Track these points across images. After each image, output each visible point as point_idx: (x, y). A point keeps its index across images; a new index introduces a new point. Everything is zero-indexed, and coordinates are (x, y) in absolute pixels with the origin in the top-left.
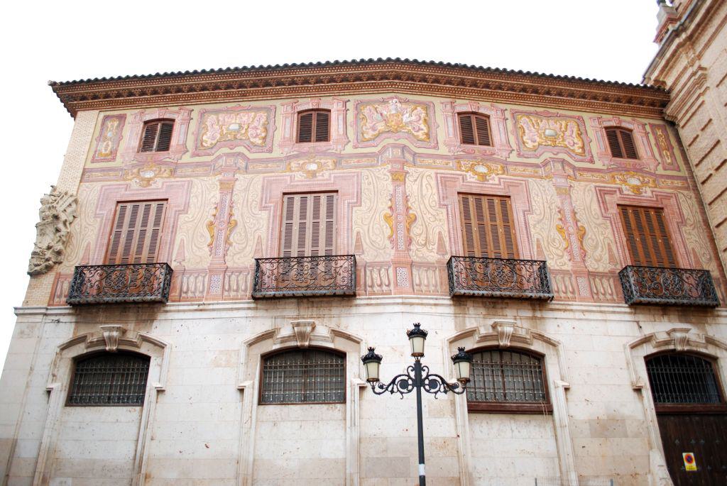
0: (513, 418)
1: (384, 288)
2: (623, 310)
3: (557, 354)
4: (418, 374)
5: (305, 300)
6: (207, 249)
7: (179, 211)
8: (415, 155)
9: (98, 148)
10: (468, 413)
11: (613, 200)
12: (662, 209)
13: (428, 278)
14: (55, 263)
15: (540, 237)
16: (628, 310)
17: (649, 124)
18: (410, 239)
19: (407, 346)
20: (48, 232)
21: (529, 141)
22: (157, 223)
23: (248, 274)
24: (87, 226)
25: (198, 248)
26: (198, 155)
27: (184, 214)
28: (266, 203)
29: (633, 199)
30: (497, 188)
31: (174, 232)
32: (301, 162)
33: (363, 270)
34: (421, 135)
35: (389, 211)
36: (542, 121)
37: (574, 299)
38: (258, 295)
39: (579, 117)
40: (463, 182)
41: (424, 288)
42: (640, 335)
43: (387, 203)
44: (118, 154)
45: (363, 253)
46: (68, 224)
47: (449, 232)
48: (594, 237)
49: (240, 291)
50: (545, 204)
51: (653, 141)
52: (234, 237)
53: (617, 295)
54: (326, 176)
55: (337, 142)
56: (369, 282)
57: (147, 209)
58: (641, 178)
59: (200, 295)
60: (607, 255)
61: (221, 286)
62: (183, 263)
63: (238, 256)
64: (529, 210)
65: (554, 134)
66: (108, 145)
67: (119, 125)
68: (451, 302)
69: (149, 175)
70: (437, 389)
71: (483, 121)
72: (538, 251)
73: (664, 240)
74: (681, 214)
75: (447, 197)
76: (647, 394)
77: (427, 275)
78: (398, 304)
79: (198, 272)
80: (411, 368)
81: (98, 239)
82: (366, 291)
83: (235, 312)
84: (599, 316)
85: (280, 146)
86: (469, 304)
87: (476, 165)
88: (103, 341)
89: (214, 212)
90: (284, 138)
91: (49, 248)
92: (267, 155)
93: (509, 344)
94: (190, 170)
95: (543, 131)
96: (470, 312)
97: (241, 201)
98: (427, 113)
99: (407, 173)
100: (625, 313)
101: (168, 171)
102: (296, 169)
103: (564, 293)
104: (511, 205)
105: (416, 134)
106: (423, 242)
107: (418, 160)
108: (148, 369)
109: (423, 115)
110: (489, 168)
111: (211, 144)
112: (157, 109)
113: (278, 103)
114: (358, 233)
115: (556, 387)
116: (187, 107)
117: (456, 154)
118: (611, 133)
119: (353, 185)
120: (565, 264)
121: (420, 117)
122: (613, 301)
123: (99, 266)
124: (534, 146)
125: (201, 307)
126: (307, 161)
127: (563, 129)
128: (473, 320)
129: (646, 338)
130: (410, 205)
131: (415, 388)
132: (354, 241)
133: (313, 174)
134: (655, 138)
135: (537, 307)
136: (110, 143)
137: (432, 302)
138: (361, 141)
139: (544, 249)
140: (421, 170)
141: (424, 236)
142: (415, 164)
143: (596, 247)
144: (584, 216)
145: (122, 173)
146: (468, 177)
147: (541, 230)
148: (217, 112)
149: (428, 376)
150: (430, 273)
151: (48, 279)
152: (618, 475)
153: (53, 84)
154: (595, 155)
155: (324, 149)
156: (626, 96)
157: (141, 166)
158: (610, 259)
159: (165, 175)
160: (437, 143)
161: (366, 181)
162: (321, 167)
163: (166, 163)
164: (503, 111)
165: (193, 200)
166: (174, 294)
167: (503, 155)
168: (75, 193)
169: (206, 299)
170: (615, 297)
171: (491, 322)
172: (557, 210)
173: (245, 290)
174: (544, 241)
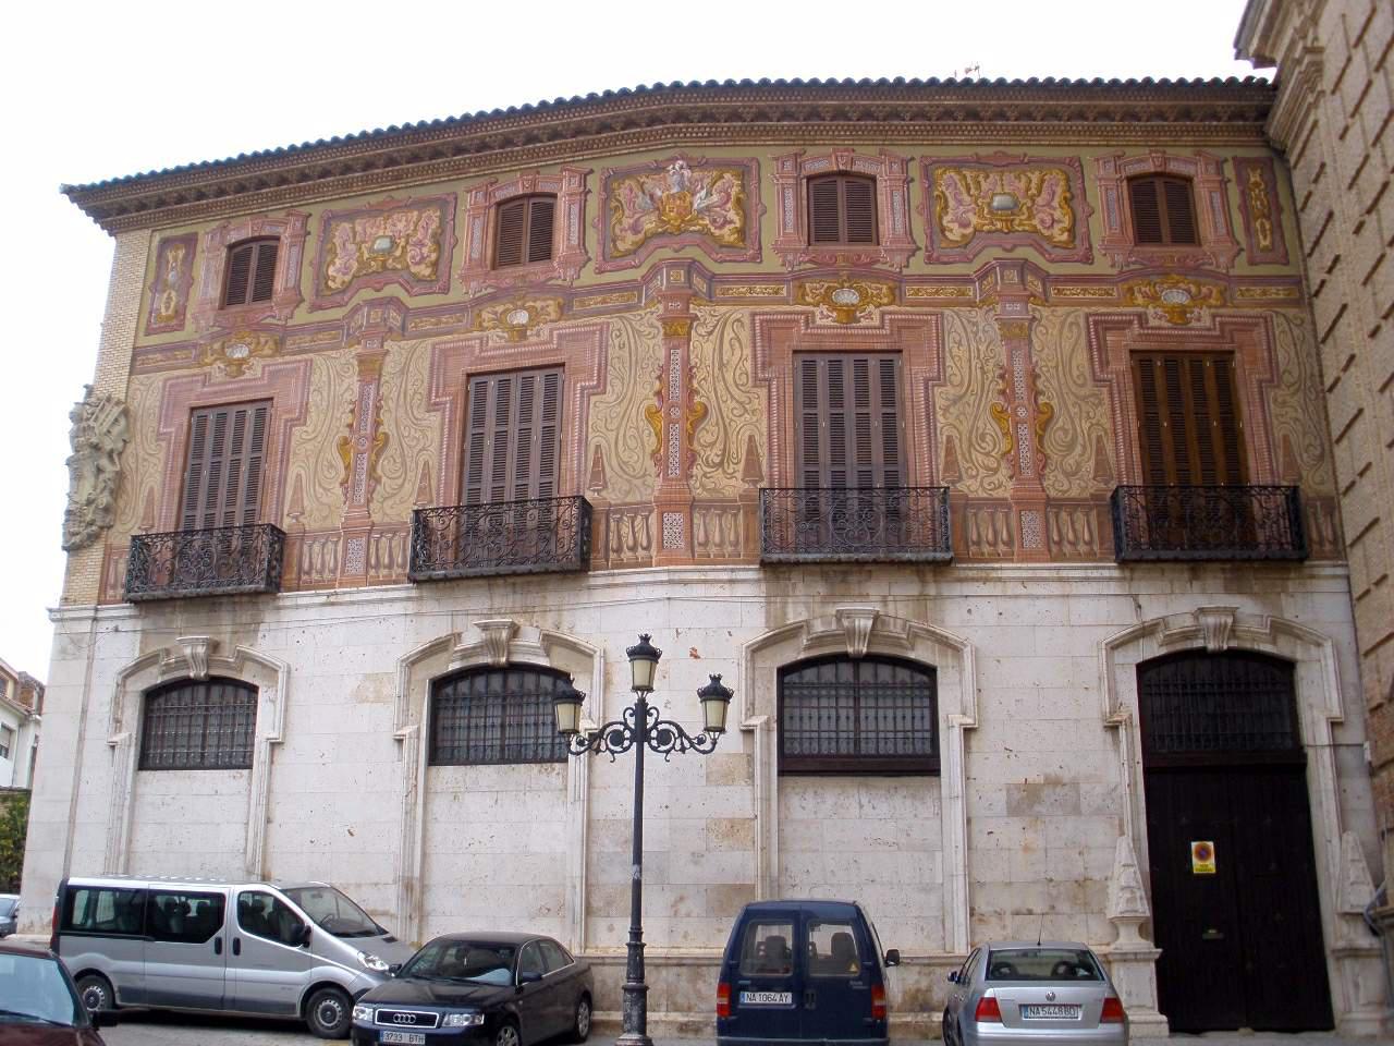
0: (867, 786)
1: (641, 553)
2: (1106, 573)
4: (641, 721)
5: (500, 581)
6: (339, 491)
7: (292, 420)
8: (712, 278)
12: (1231, 352)
13: (721, 530)
14: (102, 528)
15: (955, 433)
16: (1116, 573)
17: (1234, 159)
18: (693, 456)
19: (626, 673)
20: (86, 474)
21: (955, 226)
22: (257, 445)
25: (324, 489)
26: (320, 308)
27: (300, 425)
29: (1167, 335)
31: (285, 461)
33: (603, 521)
34: (727, 234)
35: (655, 401)
36: (987, 177)
38: (420, 576)
39: (1071, 159)
40: (807, 327)
41: (713, 550)
42: (1135, 622)
43: (652, 385)
44: (188, 316)
45: (605, 486)
46: (115, 456)
51: (1235, 198)
52: (384, 466)
53: (1101, 544)
54: (545, 335)
55: (566, 263)
56: (613, 544)
58: (1193, 289)
60: (1092, 463)
62: (301, 519)
63: (390, 502)
64: (939, 379)
66: (169, 298)
67: (187, 254)
68: (761, 575)
69: (240, 353)
70: (670, 745)
71: (862, 188)
72: (946, 463)
73: (1223, 421)
74: (1272, 363)
75: (770, 364)
76: (1132, 738)
78: (662, 582)
79: (328, 535)
82: (607, 561)
84: (1055, 589)
85: (465, 279)
86: (796, 576)
87: (835, 289)
89: (348, 418)
91: (89, 502)
92: (436, 300)
94: (308, 338)
96: (798, 593)
97: (394, 395)
98: (743, 186)
99: (696, 318)
100: (1110, 579)
101: (271, 343)
102: (491, 324)
104: (901, 368)
105: (717, 232)
106: (717, 460)
109: (734, 191)
110: (860, 291)
112: (249, 218)
114: (598, 447)
115: (950, 727)
116: (301, 209)
118: (1142, 189)
119: (593, 351)
121: (729, 195)
122: (1090, 556)
123: (167, 534)
124: (964, 236)
125: (332, 599)
128: (801, 608)
129: (1144, 628)
130: (696, 385)
133: (521, 332)
134: (1243, 193)
135: (929, 577)
136: (173, 294)
137: (725, 576)
138: (611, 258)
139: (960, 457)
140: (723, 309)
141: (718, 449)
142: (711, 298)
143: (1070, 447)
144: (1055, 384)
145: (195, 352)
147: (957, 417)
148: (350, 216)
149: (657, 723)
150: (728, 520)
151: (95, 555)
152: (1051, 880)
153: (69, 191)
154: (1096, 245)
155: (542, 278)
156: (1175, 106)
157: (226, 335)
158: (1096, 471)
159: (267, 351)
160: (760, 248)
161: (616, 342)
162: (535, 316)
163: (267, 328)
164: (905, 163)
165: (314, 398)
167: (890, 261)
168: (122, 397)
169: (341, 585)
170: (1096, 548)
172: (999, 372)
173: (403, 566)
174: (960, 440)
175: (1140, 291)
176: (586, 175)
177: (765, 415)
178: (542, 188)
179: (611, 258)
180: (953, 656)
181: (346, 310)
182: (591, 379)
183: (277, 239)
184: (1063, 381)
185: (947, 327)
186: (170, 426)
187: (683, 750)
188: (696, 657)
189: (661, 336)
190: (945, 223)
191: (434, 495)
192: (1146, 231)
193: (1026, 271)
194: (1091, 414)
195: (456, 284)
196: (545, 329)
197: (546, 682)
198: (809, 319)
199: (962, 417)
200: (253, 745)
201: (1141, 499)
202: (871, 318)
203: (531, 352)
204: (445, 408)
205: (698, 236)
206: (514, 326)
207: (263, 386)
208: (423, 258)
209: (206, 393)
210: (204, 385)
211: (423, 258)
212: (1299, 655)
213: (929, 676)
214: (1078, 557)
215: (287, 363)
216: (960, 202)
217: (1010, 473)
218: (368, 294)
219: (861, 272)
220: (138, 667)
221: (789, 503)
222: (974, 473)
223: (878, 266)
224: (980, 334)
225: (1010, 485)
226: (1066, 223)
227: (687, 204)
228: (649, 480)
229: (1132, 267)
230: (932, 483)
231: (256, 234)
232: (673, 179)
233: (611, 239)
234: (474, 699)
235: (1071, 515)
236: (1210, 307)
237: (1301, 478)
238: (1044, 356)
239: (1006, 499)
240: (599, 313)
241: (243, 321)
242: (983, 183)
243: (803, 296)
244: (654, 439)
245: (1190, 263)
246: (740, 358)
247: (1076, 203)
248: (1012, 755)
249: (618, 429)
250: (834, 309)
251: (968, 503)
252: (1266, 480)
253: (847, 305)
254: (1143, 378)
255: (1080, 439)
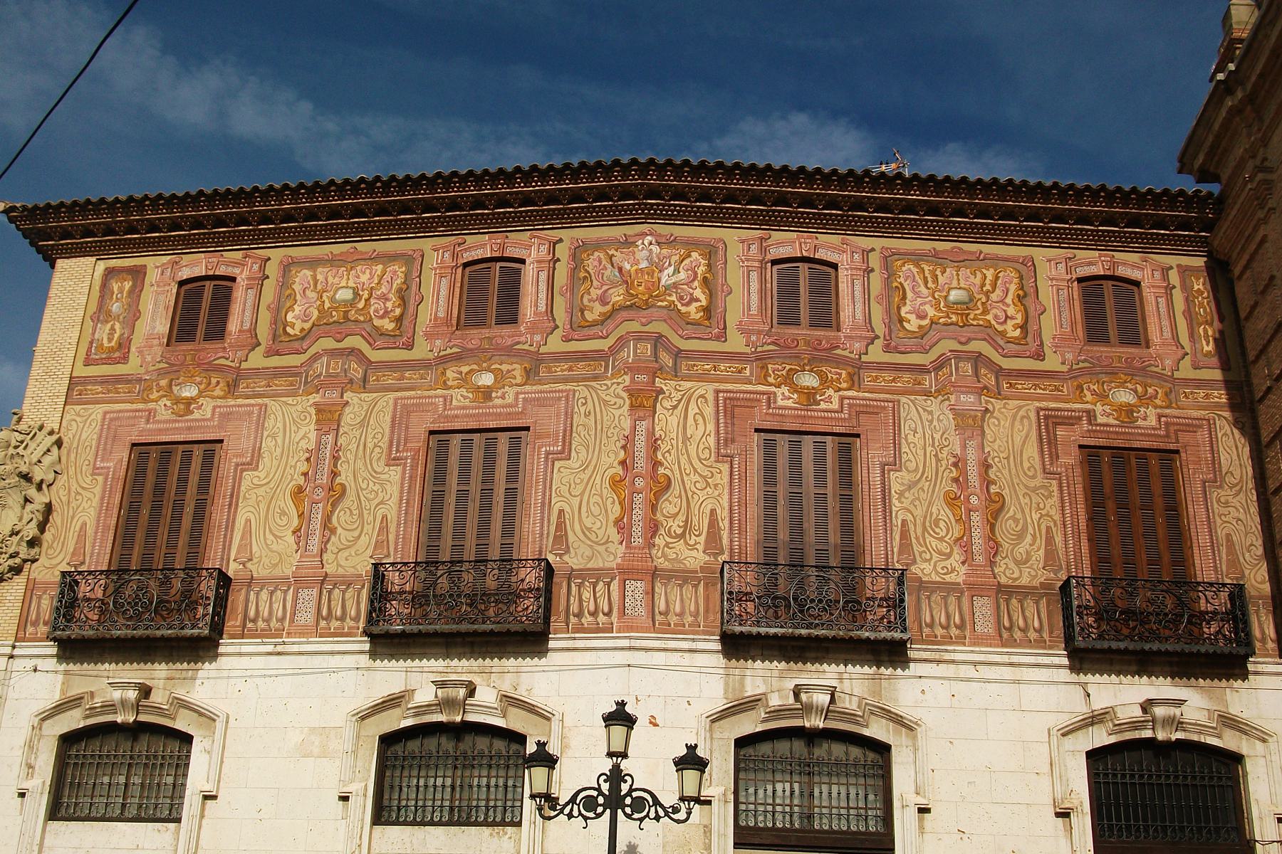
2: (1056, 660)
3: (914, 745)
4: (615, 787)
6: (291, 539)
8: (678, 354)
9: (96, 336)
10: (734, 848)
11: (1070, 437)
12: (1177, 452)
13: (682, 600)
14: (25, 561)
15: (909, 517)
17: (1179, 266)
18: (656, 526)
20: (10, 502)
21: (912, 317)
23: (363, 586)
24: (80, 490)
25: (274, 535)
26: (278, 353)
28: (397, 451)
29: (1117, 433)
30: (838, 419)
31: (233, 504)
32: (465, 369)
33: (565, 584)
34: (693, 311)
35: (619, 470)
36: (943, 272)
37: (961, 640)
39: (1025, 258)
40: (769, 407)
41: (673, 619)
43: (616, 454)
44: (133, 349)
45: (567, 551)
46: (44, 486)
47: (731, 510)
48: (1019, 516)
49: (348, 620)
50: (929, 449)
51: (1179, 304)
53: (1051, 632)
56: (574, 608)
57: (187, 458)
58: (1139, 389)
59: (278, 625)
60: (1042, 552)
61: (314, 610)
62: (249, 565)
63: (346, 553)
64: (894, 463)
65: (967, 300)
66: (113, 329)
69: (189, 392)
70: (644, 814)
72: (901, 545)
74: (1215, 462)
75: (733, 441)
76: (1083, 823)
77: (681, 595)
78: (623, 649)
79: (277, 584)
80: (604, 777)
81: (99, 517)
83: (338, 657)
84: (1007, 673)
85: (429, 336)
88: (110, 707)
89: (303, 467)
90: (436, 318)
91: (14, 533)
93: (821, 725)
95: (945, 294)
97: (353, 447)
98: (709, 265)
99: (661, 391)
100: (1060, 666)
103: (943, 627)
105: (683, 309)
106: (679, 531)
107: (684, 366)
108: (188, 757)
109: (701, 270)
111: (302, 330)
112: (203, 255)
113: (426, 244)
114: (561, 512)
117: (759, 349)
119: (558, 415)
120: (953, 570)
121: (696, 274)
122: (1040, 643)
123: (102, 572)
124: (920, 327)
125: (279, 648)
126: (475, 367)
127: (988, 287)
128: (759, 681)
130: (660, 457)
131: (608, 811)
132: (553, 528)
133: (486, 393)
134: (1187, 299)
136: (117, 326)
139: (914, 540)
140: (688, 384)
141: (682, 517)
142: (676, 374)
143: (1020, 536)
144: (1006, 472)
146: (779, 397)
147: (912, 502)
148: (313, 263)
149: (631, 790)
150: (688, 590)
154: (1047, 341)
157: (173, 372)
158: (1045, 561)
159: (218, 392)
160: (725, 328)
161: (582, 409)
162: (501, 377)
163: (220, 369)
165: (268, 444)
166: (232, 624)
168: (56, 427)
169: (289, 634)
170: (1046, 636)
171: (790, 684)
172: (952, 460)
173: (357, 619)
174: (915, 526)
175: (1089, 389)
176: (555, 244)
177: (726, 491)
178: (511, 252)
179: (578, 327)
180: (907, 736)
181: (304, 358)
182: (555, 444)
183: (233, 279)
184: (1014, 471)
185: (903, 415)
186: (108, 460)
187: (657, 818)
188: (656, 725)
189: (627, 407)
190: (903, 314)
191: (392, 549)
192: (1095, 331)
193: (980, 364)
194: (1042, 506)
195: (420, 340)
196: (510, 392)
197: (499, 745)
198: (771, 398)
199: (917, 503)
200: (182, 797)
201: (1090, 588)
202: (831, 401)
203: (496, 414)
204: (405, 464)
205: (665, 311)
206: (479, 387)
207: (214, 427)
208: (386, 312)
209: (149, 430)
210: (148, 421)
211: (386, 312)
212: (1244, 751)
213: (881, 754)
214: (1028, 643)
215: (239, 406)
216: (918, 295)
217: (963, 558)
218: (328, 343)
219: (821, 358)
220: (59, 709)
221: (750, 577)
222: (928, 557)
223: (838, 351)
224: (935, 423)
225: (963, 570)
226: (1019, 320)
227: (655, 279)
228: (612, 548)
229: (1081, 365)
230: (887, 564)
231: (211, 273)
232: (641, 254)
233: (578, 310)
234: (425, 763)
235: (1020, 601)
236: (1156, 407)
237: (1243, 576)
238: (996, 447)
239: (958, 584)
240: (566, 380)
241: (193, 360)
242: (940, 277)
243: (765, 377)
244: (617, 508)
245: (1136, 364)
246: (703, 431)
247: (1029, 302)
248: (965, 837)
249: (582, 494)
250: (796, 391)
251: (922, 585)
252: (1209, 576)
253: (808, 388)
254: (1091, 473)
255: (1030, 530)
